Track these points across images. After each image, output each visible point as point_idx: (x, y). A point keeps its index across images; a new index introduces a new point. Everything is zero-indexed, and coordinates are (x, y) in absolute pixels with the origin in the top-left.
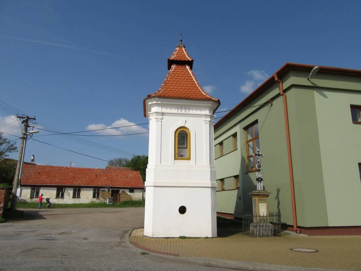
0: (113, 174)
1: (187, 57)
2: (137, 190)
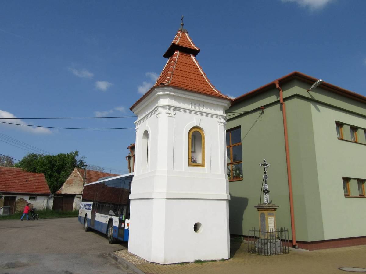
0: (8, 176)
1: (192, 45)
2: (41, 197)
